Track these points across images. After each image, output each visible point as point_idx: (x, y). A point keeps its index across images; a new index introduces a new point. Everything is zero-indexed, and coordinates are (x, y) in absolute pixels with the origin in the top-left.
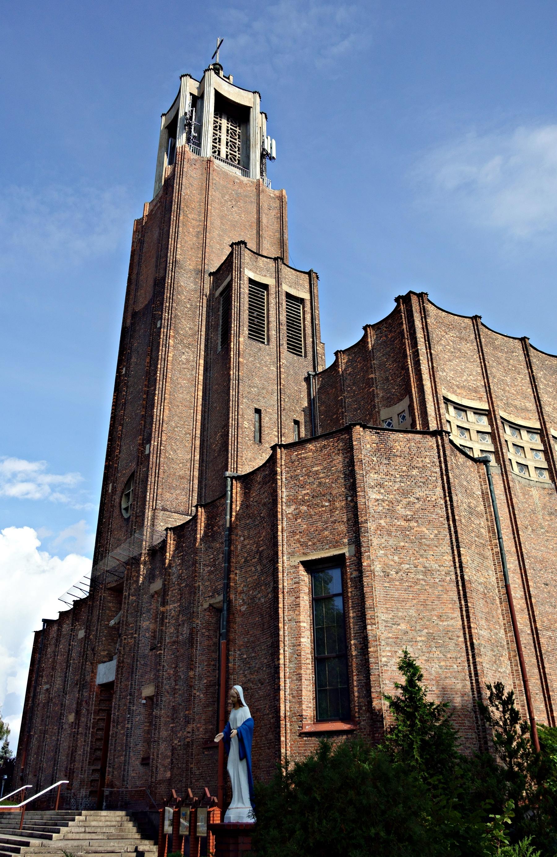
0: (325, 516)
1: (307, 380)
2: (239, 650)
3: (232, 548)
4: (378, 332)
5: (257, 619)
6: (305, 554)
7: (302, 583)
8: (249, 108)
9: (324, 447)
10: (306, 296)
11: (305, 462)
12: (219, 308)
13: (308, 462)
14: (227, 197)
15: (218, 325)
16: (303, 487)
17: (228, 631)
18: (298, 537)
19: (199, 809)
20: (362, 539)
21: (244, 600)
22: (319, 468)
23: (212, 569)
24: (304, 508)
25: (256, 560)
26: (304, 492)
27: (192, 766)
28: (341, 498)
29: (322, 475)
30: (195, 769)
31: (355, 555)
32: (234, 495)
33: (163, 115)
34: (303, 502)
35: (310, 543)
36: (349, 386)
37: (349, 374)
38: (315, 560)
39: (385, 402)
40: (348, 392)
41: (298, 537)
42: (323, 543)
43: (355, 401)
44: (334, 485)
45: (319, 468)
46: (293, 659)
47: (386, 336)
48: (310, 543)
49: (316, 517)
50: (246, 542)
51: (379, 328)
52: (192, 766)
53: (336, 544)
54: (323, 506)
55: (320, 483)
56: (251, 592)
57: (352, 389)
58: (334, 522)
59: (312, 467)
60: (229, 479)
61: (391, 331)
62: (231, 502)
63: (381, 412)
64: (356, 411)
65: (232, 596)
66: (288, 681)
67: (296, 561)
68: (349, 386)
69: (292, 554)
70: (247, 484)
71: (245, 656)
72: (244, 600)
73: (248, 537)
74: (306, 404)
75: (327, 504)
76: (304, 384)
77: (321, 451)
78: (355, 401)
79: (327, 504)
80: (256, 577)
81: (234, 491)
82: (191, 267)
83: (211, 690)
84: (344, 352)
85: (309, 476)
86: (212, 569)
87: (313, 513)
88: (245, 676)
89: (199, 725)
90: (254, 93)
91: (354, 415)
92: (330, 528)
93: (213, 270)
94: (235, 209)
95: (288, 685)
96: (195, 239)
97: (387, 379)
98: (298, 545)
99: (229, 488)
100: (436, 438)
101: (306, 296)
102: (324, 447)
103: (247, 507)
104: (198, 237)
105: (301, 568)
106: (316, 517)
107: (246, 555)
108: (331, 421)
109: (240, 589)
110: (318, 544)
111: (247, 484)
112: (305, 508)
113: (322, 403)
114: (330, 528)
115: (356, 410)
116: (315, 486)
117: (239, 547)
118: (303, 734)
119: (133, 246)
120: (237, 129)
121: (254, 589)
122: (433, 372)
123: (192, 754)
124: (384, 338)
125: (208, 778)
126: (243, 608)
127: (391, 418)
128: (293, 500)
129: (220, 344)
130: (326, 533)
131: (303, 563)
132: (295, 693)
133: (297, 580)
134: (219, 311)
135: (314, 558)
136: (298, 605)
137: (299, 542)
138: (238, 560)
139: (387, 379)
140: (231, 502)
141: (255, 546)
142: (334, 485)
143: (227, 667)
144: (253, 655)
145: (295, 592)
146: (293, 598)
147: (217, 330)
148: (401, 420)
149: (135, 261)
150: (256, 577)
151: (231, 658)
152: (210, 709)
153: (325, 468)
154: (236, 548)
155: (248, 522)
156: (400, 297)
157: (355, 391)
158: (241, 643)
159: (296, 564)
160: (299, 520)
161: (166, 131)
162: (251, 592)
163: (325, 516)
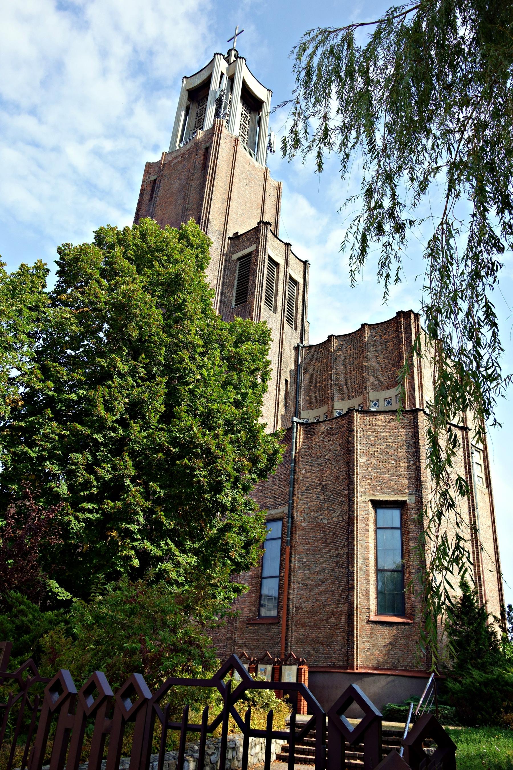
0: (392, 471)
1: (297, 349)
2: (299, 555)
3: (296, 477)
4: (373, 331)
5: (318, 534)
6: (374, 495)
7: (370, 515)
8: (263, 102)
9: (392, 419)
10: (301, 281)
11: (375, 427)
12: (235, 270)
13: (379, 428)
14: (243, 175)
15: (233, 284)
16: (374, 445)
17: (291, 539)
18: (369, 481)
19: (283, 667)
20: (423, 493)
21: (304, 518)
22: (387, 434)
23: (261, 488)
24: (374, 461)
25: (318, 490)
26: (374, 449)
27: (236, 636)
28: (405, 460)
29: (389, 440)
30: (238, 639)
31: (415, 503)
32: (298, 437)
33: (186, 77)
34: (373, 456)
35: (378, 488)
36: (338, 365)
37: (339, 356)
38: (382, 501)
39: (374, 387)
40: (337, 369)
41: (369, 481)
42: (390, 490)
43: (343, 378)
44: (399, 450)
45: (387, 434)
46: (363, 568)
47: (380, 336)
48: (378, 488)
49: (384, 470)
50: (308, 475)
51: (374, 329)
52: (236, 636)
53: (400, 493)
54: (390, 463)
55: (388, 446)
56: (312, 514)
57: (340, 368)
58: (399, 476)
59: (382, 432)
60: (295, 424)
61: (385, 334)
62: (296, 441)
63: (370, 394)
64: (343, 386)
65: (295, 514)
66: (359, 583)
67: (367, 498)
68: (338, 365)
69: (364, 493)
70: (309, 430)
71: (305, 560)
72: (304, 518)
73: (310, 472)
74: (293, 368)
75: (393, 462)
76: (293, 351)
77: (389, 422)
78: (343, 378)
79: (393, 462)
80: (318, 503)
81: (298, 433)
82: (216, 228)
83: (255, 581)
84: (336, 337)
85: (378, 439)
86: (261, 488)
87: (381, 466)
88: (305, 575)
89: (243, 606)
90: (269, 90)
91: (340, 389)
92: (395, 480)
93: (231, 236)
94: (247, 187)
95: (359, 586)
96: (220, 204)
97: (377, 369)
98: (369, 487)
99: (295, 431)
100: (462, 432)
101: (301, 281)
102: (392, 419)
103: (309, 448)
104: (223, 204)
105: (370, 504)
106: (384, 470)
107: (307, 485)
108: (314, 387)
109: (301, 509)
110: (385, 490)
111: (309, 430)
112: (375, 462)
113: (307, 371)
114: (395, 480)
115: (342, 385)
116: (384, 447)
117: (301, 477)
118: (369, 622)
119: (143, 185)
120: (248, 115)
121: (316, 511)
122: (421, 375)
123: (236, 628)
124: (378, 337)
125: (252, 647)
126: (304, 524)
127: (378, 401)
128: (366, 454)
129: (234, 301)
130: (392, 483)
131: (372, 501)
132: (364, 593)
133: (367, 512)
134: (235, 272)
135: (381, 499)
136: (368, 530)
137: (370, 485)
138: (301, 487)
139: (377, 369)
140: (296, 441)
141: (317, 479)
142: (399, 450)
143: (290, 566)
144: (313, 560)
145: (366, 521)
146: (364, 525)
147: (233, 288)
148: (386, 403)
149: (144, 199)
150: (318, 503)
151: (293, 560)
152: (254, 595)
153: (392, 436)
154: (298, 477)
155: (310, 460)
156: (402, 312)
157: (342, 370)
158: (301, 550)
159: (367, 500)
160: (370, 469)
161: (187, 93)
162: (312, 514)
163: (392, 471)
